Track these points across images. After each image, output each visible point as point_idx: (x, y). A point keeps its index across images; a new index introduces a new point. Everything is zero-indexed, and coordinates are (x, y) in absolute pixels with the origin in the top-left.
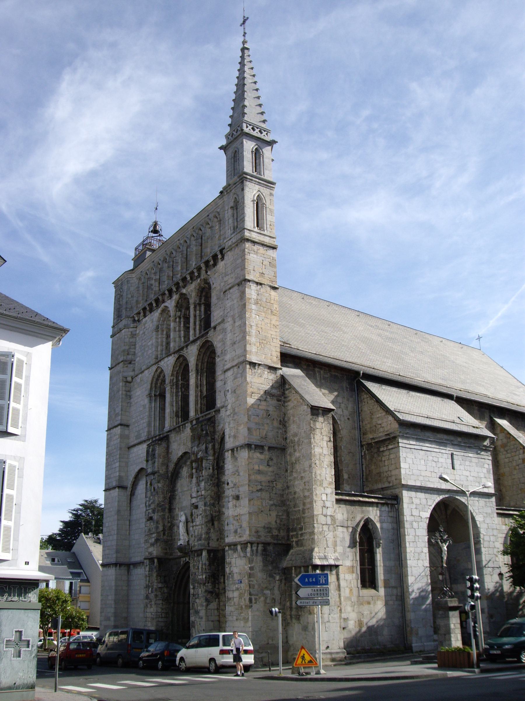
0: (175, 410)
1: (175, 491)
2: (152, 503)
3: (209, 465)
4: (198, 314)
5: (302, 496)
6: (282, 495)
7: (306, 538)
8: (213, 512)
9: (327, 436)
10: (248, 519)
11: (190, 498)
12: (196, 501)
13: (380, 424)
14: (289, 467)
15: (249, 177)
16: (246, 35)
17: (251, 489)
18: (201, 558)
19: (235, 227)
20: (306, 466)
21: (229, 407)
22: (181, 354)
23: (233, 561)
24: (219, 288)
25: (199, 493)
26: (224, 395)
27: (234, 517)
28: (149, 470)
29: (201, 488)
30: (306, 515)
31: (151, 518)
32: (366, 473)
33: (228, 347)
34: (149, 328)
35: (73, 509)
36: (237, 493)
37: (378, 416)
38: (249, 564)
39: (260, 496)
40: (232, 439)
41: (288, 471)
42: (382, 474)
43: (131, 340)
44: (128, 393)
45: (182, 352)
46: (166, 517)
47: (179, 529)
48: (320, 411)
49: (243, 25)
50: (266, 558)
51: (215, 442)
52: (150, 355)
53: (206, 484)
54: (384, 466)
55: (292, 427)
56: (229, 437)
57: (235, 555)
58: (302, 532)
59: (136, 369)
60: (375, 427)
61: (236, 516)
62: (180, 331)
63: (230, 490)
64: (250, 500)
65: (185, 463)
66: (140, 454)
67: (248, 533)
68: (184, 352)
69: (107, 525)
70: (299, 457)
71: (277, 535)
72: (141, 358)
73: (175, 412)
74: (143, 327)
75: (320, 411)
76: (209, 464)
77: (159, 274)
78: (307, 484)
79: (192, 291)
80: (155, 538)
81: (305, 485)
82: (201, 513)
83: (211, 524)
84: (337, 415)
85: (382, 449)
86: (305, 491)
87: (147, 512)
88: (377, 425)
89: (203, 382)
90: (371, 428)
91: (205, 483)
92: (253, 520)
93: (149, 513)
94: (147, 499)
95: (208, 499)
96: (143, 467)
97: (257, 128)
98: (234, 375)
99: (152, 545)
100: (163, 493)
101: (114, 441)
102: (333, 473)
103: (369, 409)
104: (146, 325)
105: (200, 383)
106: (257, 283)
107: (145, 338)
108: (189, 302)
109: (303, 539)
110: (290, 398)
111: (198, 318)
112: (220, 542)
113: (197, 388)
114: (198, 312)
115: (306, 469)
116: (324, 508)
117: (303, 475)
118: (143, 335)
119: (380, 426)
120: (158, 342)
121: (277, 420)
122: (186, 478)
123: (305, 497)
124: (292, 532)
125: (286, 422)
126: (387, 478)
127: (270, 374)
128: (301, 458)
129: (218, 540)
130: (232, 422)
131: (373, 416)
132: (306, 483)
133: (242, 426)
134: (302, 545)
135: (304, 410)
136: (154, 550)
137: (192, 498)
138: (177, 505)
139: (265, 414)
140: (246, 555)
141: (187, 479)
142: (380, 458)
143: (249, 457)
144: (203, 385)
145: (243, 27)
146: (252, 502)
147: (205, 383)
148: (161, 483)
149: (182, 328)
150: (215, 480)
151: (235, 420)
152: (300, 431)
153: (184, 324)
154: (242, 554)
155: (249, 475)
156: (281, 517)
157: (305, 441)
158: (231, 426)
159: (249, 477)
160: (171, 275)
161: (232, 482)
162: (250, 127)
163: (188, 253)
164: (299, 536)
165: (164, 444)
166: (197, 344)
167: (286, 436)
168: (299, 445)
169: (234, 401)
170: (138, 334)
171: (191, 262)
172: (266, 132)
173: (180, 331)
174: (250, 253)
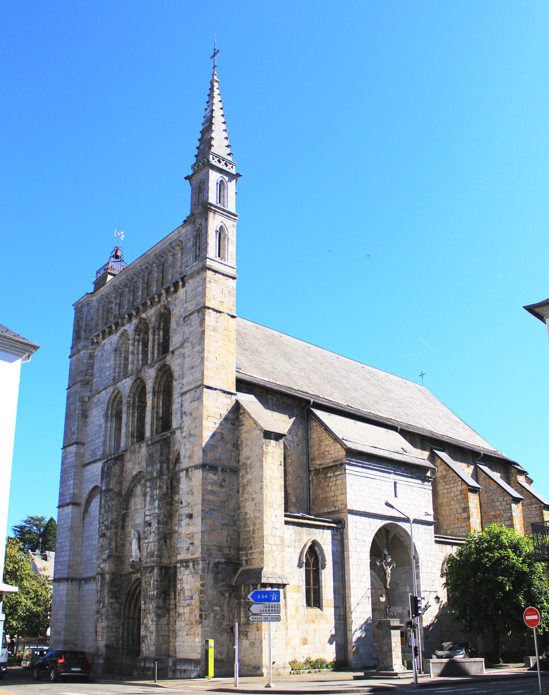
0: (130, 430)
2: (105, 520)
8: (165, 530)
13: (328, 451)
14: (241, 489)
31: (103, 535)
34: (108, 350)
36: (191, 512)
40: (187, 460)
42: (329, 499)
46: (119, 534)
52: (108, 376)
56: (184, 458)
57: (187, 572)
58: (252, 551)
61: (189, 534)
62: (138, 354)
63: (184, 508)
66: (95, 473)
70: (251, 480)
71: (228, 554)
72: (99, 379)
73: (130, 432)
74: (102, 349)
76: (163, 483)
79: (151, 316)
81: (256, 506)
82: (154, 530)
85: (329, 475)
88: (325, 452)
90: (319, 454)
94: (101, 516)
95: (161, 517)
99: (105, 561)
104: (105, 347)
110: (244, 422)
111: (156, 342)
113: (154, 410)
117: (254, 496)
118: (101, 357)
121: (231, 443)
130: (187, 443)
131: (321, 444)
143: (203, 478)
144: (159, 406)
146: (204, 521)
153: (143, 348)
158: (186, 447)
161: (186, 501)
162: (216, 159)
164: (249, 555)
165: (119, 463)
169: (190, 423)
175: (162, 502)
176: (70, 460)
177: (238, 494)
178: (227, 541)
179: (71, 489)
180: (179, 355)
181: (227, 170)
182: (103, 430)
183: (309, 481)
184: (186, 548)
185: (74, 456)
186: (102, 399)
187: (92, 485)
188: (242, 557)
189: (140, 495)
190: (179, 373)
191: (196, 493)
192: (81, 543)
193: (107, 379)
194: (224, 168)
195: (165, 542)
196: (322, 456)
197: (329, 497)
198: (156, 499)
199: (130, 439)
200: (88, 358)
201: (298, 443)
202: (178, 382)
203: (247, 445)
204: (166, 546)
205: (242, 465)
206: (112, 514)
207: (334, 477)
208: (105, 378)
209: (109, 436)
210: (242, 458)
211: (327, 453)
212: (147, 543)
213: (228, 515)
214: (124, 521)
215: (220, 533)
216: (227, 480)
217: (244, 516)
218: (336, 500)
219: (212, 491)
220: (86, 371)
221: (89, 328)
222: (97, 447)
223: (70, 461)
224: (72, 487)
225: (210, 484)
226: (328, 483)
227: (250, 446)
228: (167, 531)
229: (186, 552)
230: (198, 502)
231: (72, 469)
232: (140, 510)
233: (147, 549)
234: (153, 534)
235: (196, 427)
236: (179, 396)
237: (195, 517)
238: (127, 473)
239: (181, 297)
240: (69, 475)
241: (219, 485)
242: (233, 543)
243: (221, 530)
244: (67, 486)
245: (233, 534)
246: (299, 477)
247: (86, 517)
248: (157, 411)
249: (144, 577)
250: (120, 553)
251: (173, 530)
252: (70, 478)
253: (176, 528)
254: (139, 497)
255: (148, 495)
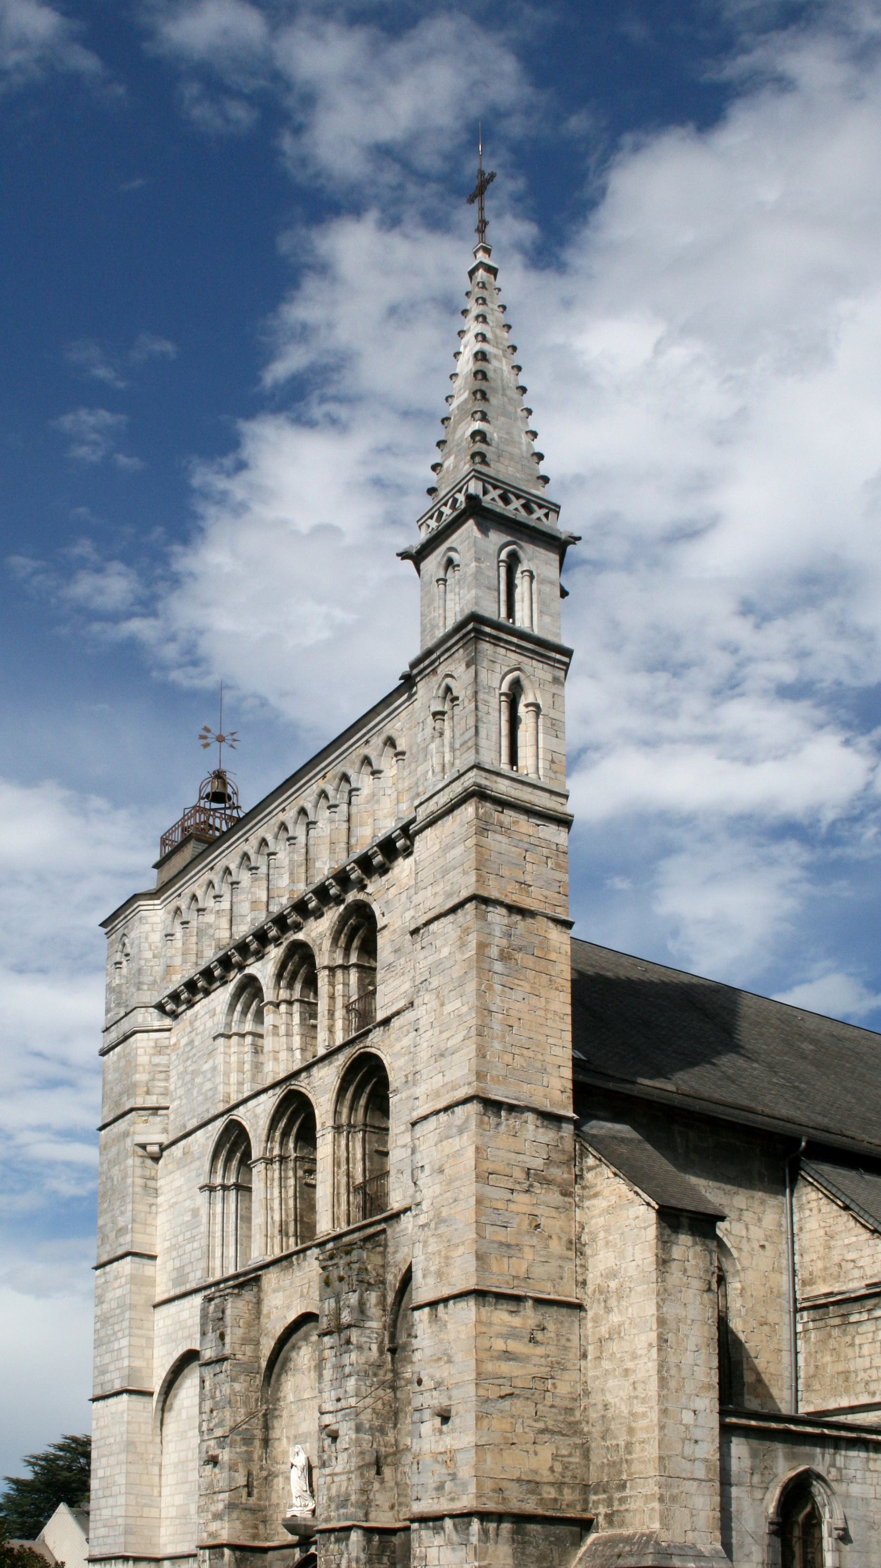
0: (277, 1218)
1: (278, 1400)
2: (216, 1426)
3: (368, 1340)
4: (341, 993)
5: (626, 1413)
6: (570, 1411)
7: (633, 1506)
8: (379, 1445)
9: (701, 1278)
10: (473, 1461)
11: (319, 1415)
12: (334, 1421)
13: (853, 1261)
14: (590, 1349)
15: (487, 630)
16: (489, 230)
17: (482, 1392)
18: (347, 1545)
19: (447, 766)
20: (639, 1347)
21: (425, 1206)
22: (292, 1087)
23: (432, 1553)
24: (400, 923)
25: (343, 1404)
26: (410, 1181)
27: (436, 1455)
28: (208, 1354)
29: (346, 1391)
30: (634, 1456)
31: (213, 1461)
32: (806, 1372)
33: (422, 1065)
34: (204, 1031)
35: (29, 1454)
36: (445, 1403)
37: (846, 1242)
38: (476, 1560)
39: (508, 1408)
40: (431, 1281)
41: (589, 1357)
42: (853, 1375)
43: (156, 1060)
44: (151, 1183)
45: (296, 1083)
46: (256, 1457)
47: (289, 1484)
48: (685, 1221)
49: (477, 201)
50: (524, 1548)
51: (385, 1289)
52: (210, 1094)
53: (360, 1383)
54: (860, 1357)
55: (602, 1255)
56: (424, 1276)
57: (439, 1540)
58: (624, 1494)
59: (170, 1128)
60: (837, 1268)
61: (441, 1453)
62: (289, 1035)
63: (426, 1394)
64: (478, 1419)
65: (306, 1338)
66: (185, 1320)
67: (475, 1491)
68: (302, 1084)
69: (100, 1473)
70: (620, 1326)
71: (555, 1500)
72: (184, 1101)
73: (277, 1224)
74: (188, 1029)
75: (685, 1221)
76: (370, 1338)
77: (229, 899)
78: (640, 1386)
79: (321, 936)
80: (226, 1502)
81: (635, 1388)
82: (347, 1446)
83: (373, 1472)
84: (731, 1237)
85: (854, 1318)
86: (635, 1401)
87: (205, 1445)
88: (843, 1264)
89: (354, 1154)
90: (825, 1269)
91: (357, 1380)
92: (488, 1463)
93: (208, 1447)
94: (205, 1417)
95: (366, 1417)
96: (193, 1347)
97: (518, 497)
98: (437, 1131)
99: (217, 1516)
100: (246, 1404)
101: (114, 1289)
102: (715, 1363)
103: (823, 1224)
104: (197, 1024)
105: (345, 1154)
106: (513, 909)
107: (194, 1055)
108: (313, 965)
109: (627, 1510)
110: (598, 1189)
111: (339, 1002)
112: (398, 1512)
113: (339, 1167)
114: (339, 988)
115: (639, 1352)
116: (687, 1442)
117: (630, 1365)
118: (189, 1048)
119: (853, 1264)
120: (229, 1063)
121: (560, 1238)
122: (309, 1372)
123: (632, 1414)
124: (596, 1493)
125: (584, 1245)
126: (867, 1384)
127: (541, 1130)
128: (627, 1326)
129: (392, 1507)
130: (431, 1240)
131: (832, 1243)
132: (636, 1385)
133: (461, 1250)
134: (622, 1524)
135: (637, 1217)
136: (223, 1528)
137: (322, 1413)
138: (281, 1430)
139: (527, 1222)
140: (468, 1540)
141: (312, 1372)
142: (848, 1339)
143: (479, 1322)
144: (355, 1159)
145: (476, 205)
146: (485, 1422)
147: (359, 1155)
148: (241, 1381)
149: (296, 1029)
150: (385, 1375)
151: (440, 1236)
152: (623, 1266)
153: (303, 1019)
154: (455, 1538)
155: (479, 1362)
156: (566, 1459)
157: (639, 1289)
158: (430, 1249)
159: (477, 1366)
160: (264, 899)
161: (432, 1378)
162: (495, 494)
163: (311, 842)
164: (616, 1503)
165: (248, 1295)
166: (337, 1063)
167: (584, 1277)
168: (620, 1298)
169: (438, 1192)
170: (175, 1045)
171: (318, 864)
172: (545, 511)
173: (289, 1035)
174: (488, 830)
175: (368, 1383)
176: (119, 1292)
177: (583, 1362)
178: (552, 1469)
179: (123, 1359)
180: (405, 1029)
181: (532, 524)
182: (205, 1220)
183: (796, 1333)
184: (434, 1485)
185: (126, 1284)
186: (195, 1148)
187: (180, 1348)
188: (597, 1508)
189: (310, 1367)
190: (404, 1073)
191: (458, 1358)
192: (157, 1478)
193: (206, 1099)
194: (522, 516)
195: (378, 1473)
196: (836, 1273)
197: (856, 1372)
198: (350, 1375)
199: (277, 1240)
200: (152, 1051)
201: (762, 1243)
202: (404, 1095)
203: (607, 1243)
204: (382, 1482)
205: (595, 1291)
206: (234, 1414)
207: (868, 1323)
208: (200, 1098)
209: (218, 1234)
210: (593, 1277)
211: (851, 1265)
212: (329, 1475)
213: (553, 1410)
214: (267, 1427)
215: (531, 1452)
216: (551, 1327)
217: (602, 1413)
218: (874, 1378)
219: (506, 1352)
220: (147, 1083)
221: (151, 978)
222: (188, 1261)
223: (117, 1296)
224: (125, 1352)
225: (499, 1335)
226: (853, 1337)
227: (615, 1246)
228: (383, 1449)
229: (434, 1494)
230: (467, 1378)
231: (123, 1312)
232: (311, 1403)
233: (329, 1489)
234: (345, 1455)
235: (455, 1200)
236: (406, 1130)
237: (457, 1413)
238: (272, 1317)
239: (405, 881)
240: (117, 1327)
241: (527, 1340)
242: (569, 1473)
243: (534, 1443)
244: (113, 1351)
245: (570, 1455)
246: (766, 1324)
247: (166, 1421)
248: (348, 1169)
249: (323, 1552)
250: (259, 1499)
251: (401, 1447)
252: (120, 1334)
253: (408, 1441)
254: (306, 1373)
255: (329, 1365)
